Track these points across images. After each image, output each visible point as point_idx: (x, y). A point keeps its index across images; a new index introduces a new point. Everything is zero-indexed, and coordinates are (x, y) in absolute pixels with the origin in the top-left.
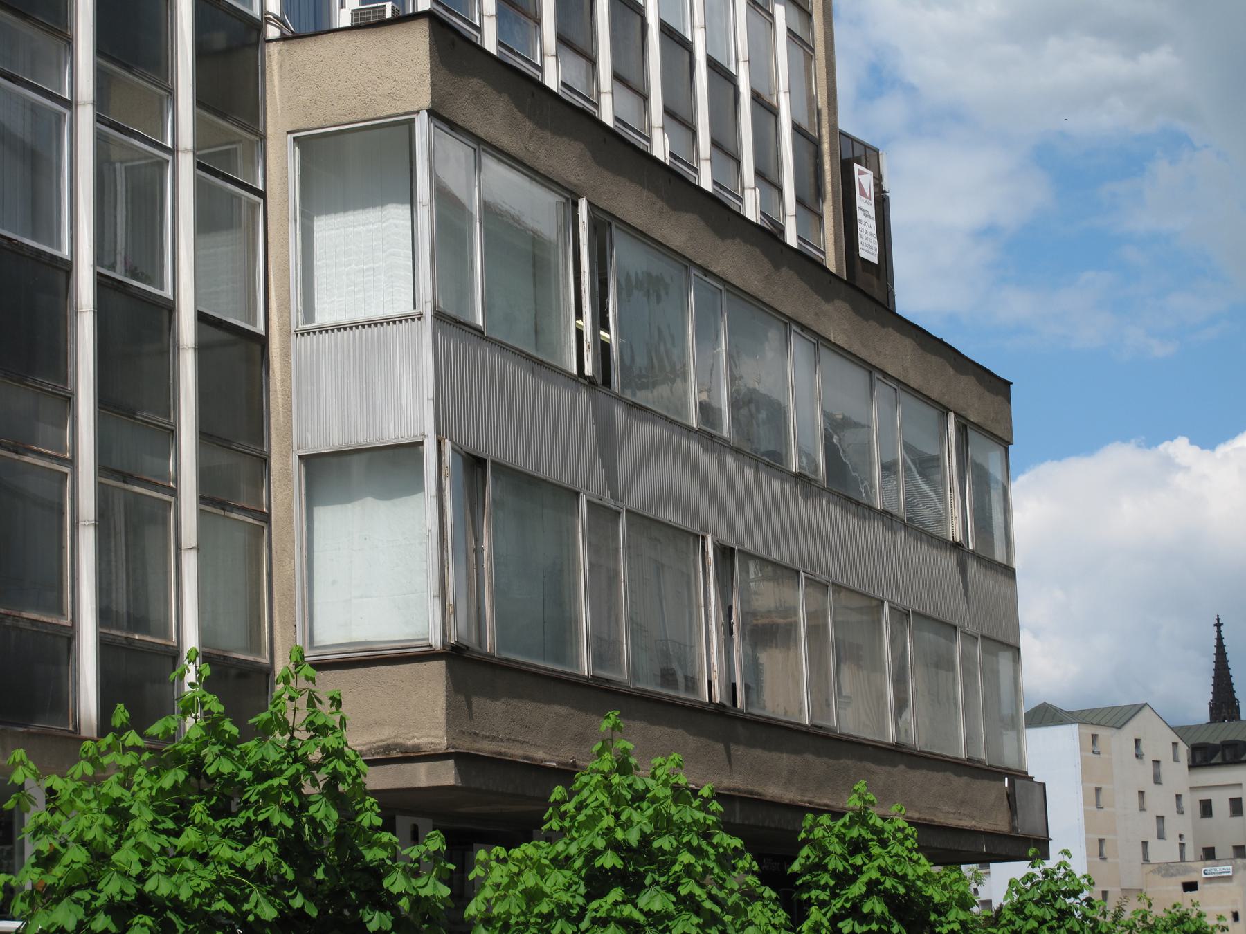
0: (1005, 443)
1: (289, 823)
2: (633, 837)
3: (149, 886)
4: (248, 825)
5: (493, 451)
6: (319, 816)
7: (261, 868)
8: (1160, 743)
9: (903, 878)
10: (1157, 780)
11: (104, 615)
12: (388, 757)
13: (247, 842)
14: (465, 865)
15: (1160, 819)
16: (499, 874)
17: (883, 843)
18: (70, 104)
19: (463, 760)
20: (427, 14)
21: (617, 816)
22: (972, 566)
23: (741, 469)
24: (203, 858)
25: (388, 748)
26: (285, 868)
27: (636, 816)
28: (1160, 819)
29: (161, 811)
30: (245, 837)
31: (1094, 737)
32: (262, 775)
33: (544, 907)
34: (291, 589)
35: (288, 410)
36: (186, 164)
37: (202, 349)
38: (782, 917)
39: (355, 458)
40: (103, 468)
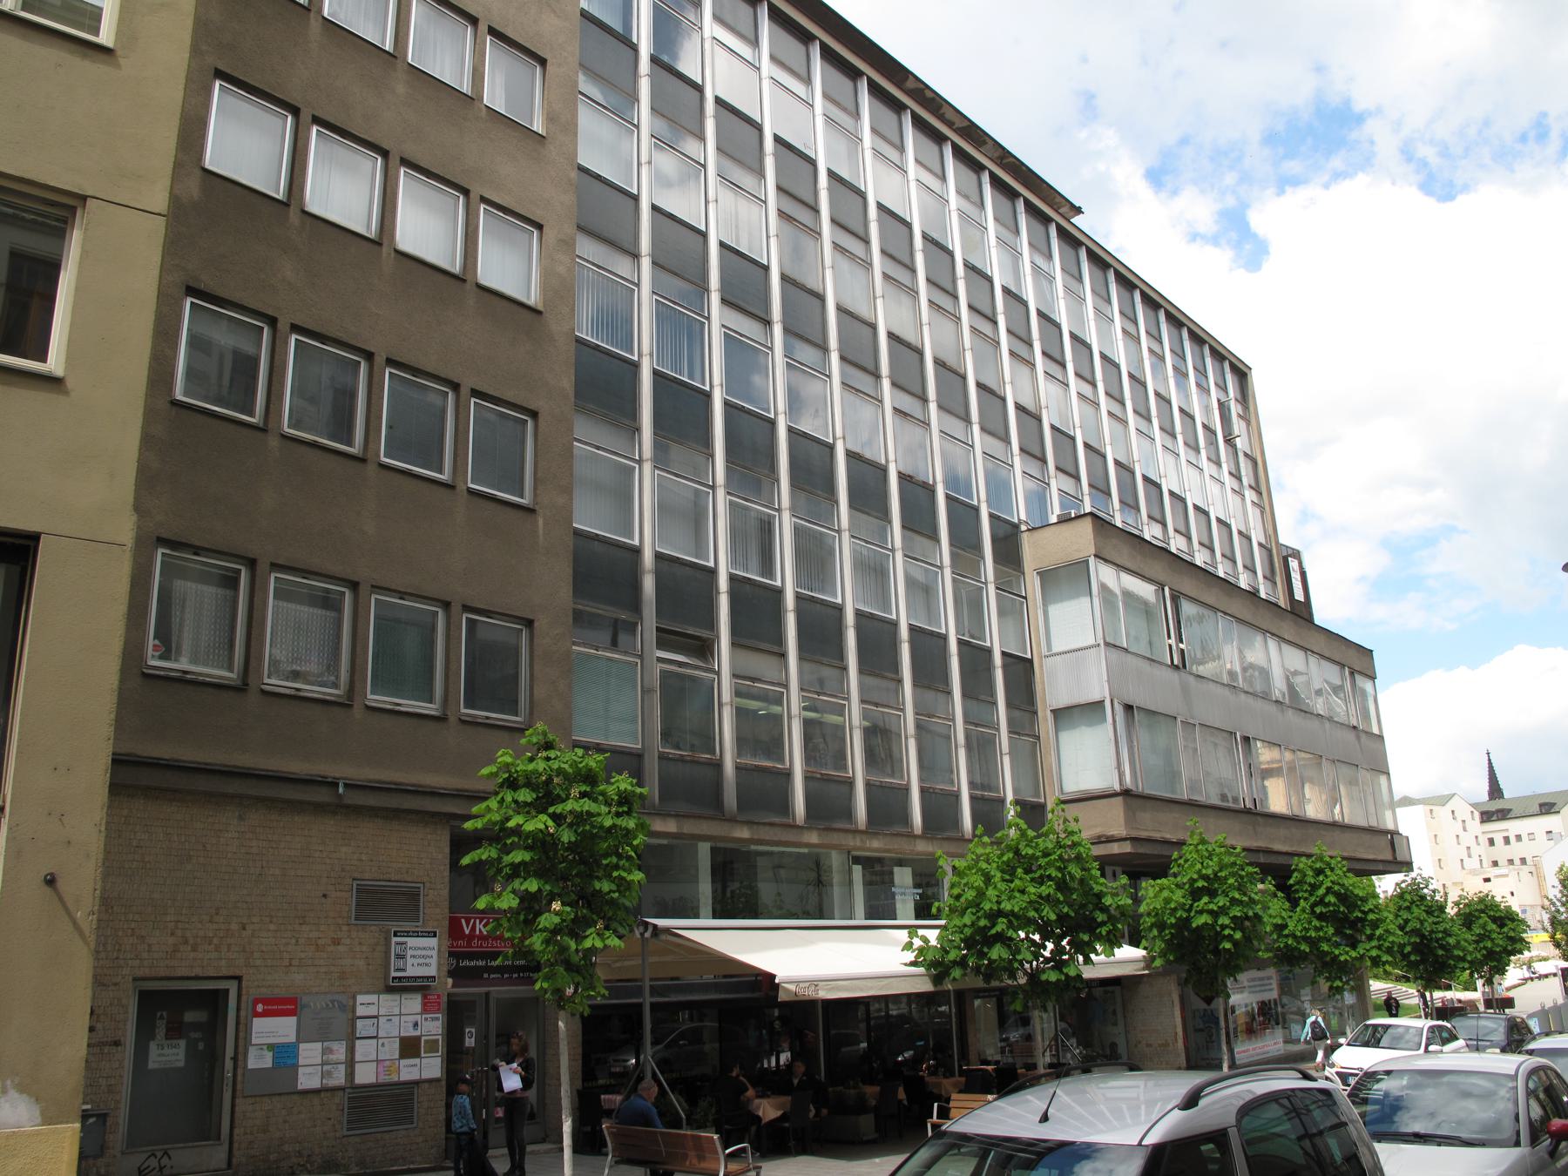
0: (1373, 678)
1: (1060, 875)
2: (1209, 871)
3: (1002, 906)
4: (1041, 877)
5: (1136, 701)
6: (1073, 871)
7: (1049, 895)
8: (1464, 811)
9: (1343, 885)
10: (1465, 830)
11: (972, 785)
12: (1100, 840)
13: (1042, 884)
14: (1137, 888)
15: (1468, 848)
16: (1151, 893)
17: (1332, 870)
18: (941, 568)
19: (1134, 840)
20: (1091, 514)
21: (1202, 863)
22: (1363, 737)
23: (1250, 700)
24: (1023, 892)
25: (1099, 837)
26: (1059, 895)
27: (1211, 863)
28: (1468, 848)
29: (1003, 871)
30: (1041, 881)
31: (1431, 810)
32: (1046, 854)
33: (1173, 905)
34: (1051, 768)
35: (1043, 683)
36: (992, 588)
37: (1005, 667)
38: (1287, 905)
39: (1075, 710)
40: (966, 722)
